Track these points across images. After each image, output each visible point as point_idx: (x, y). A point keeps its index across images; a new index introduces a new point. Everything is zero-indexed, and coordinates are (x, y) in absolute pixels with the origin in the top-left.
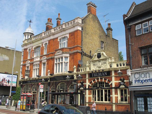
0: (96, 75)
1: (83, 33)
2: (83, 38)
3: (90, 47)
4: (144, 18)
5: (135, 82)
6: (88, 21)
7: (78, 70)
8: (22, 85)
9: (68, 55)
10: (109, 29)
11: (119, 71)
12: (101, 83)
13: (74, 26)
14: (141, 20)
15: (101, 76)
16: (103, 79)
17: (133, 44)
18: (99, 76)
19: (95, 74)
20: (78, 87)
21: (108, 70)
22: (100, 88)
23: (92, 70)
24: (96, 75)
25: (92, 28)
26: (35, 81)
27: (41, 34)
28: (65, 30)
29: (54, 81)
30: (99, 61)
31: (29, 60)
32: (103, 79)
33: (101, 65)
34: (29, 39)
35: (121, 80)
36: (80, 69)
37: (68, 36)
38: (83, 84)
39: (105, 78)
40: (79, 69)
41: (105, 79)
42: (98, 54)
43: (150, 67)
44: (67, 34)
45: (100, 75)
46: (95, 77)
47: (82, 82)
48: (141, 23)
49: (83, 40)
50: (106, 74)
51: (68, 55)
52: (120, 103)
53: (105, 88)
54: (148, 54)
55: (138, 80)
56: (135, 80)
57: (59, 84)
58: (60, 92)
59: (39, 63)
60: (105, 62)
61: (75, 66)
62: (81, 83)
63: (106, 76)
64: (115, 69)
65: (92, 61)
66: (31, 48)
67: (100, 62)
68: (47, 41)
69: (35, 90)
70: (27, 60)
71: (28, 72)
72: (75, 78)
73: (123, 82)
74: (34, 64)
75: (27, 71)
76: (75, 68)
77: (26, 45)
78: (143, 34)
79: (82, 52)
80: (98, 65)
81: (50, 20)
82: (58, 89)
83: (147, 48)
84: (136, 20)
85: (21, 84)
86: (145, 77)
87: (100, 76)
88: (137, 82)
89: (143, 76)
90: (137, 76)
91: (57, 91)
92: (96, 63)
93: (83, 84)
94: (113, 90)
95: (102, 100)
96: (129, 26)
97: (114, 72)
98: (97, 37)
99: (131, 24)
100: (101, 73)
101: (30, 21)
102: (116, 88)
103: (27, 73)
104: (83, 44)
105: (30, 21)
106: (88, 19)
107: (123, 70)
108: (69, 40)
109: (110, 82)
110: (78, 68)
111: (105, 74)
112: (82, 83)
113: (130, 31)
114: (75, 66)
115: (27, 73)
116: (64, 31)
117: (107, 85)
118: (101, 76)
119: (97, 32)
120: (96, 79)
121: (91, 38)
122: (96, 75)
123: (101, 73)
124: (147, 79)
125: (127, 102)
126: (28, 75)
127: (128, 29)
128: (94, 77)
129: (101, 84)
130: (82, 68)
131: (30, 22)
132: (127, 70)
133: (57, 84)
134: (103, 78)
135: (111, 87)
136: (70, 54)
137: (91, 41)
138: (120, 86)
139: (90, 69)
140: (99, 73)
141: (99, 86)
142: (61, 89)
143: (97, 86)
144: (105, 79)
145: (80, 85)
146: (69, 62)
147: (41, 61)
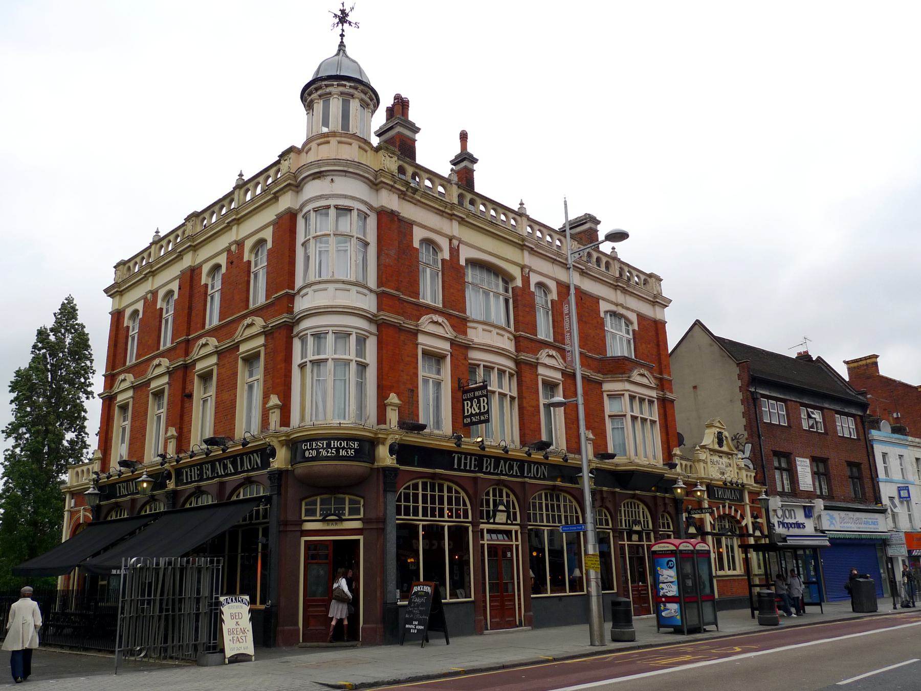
19: (487, 461)
30: (720, 453)
50: (546, 474)
67: (721, 457)
69: (508, 517)
80: (721, 466)
101: (343, 11)
126: (480, 414)
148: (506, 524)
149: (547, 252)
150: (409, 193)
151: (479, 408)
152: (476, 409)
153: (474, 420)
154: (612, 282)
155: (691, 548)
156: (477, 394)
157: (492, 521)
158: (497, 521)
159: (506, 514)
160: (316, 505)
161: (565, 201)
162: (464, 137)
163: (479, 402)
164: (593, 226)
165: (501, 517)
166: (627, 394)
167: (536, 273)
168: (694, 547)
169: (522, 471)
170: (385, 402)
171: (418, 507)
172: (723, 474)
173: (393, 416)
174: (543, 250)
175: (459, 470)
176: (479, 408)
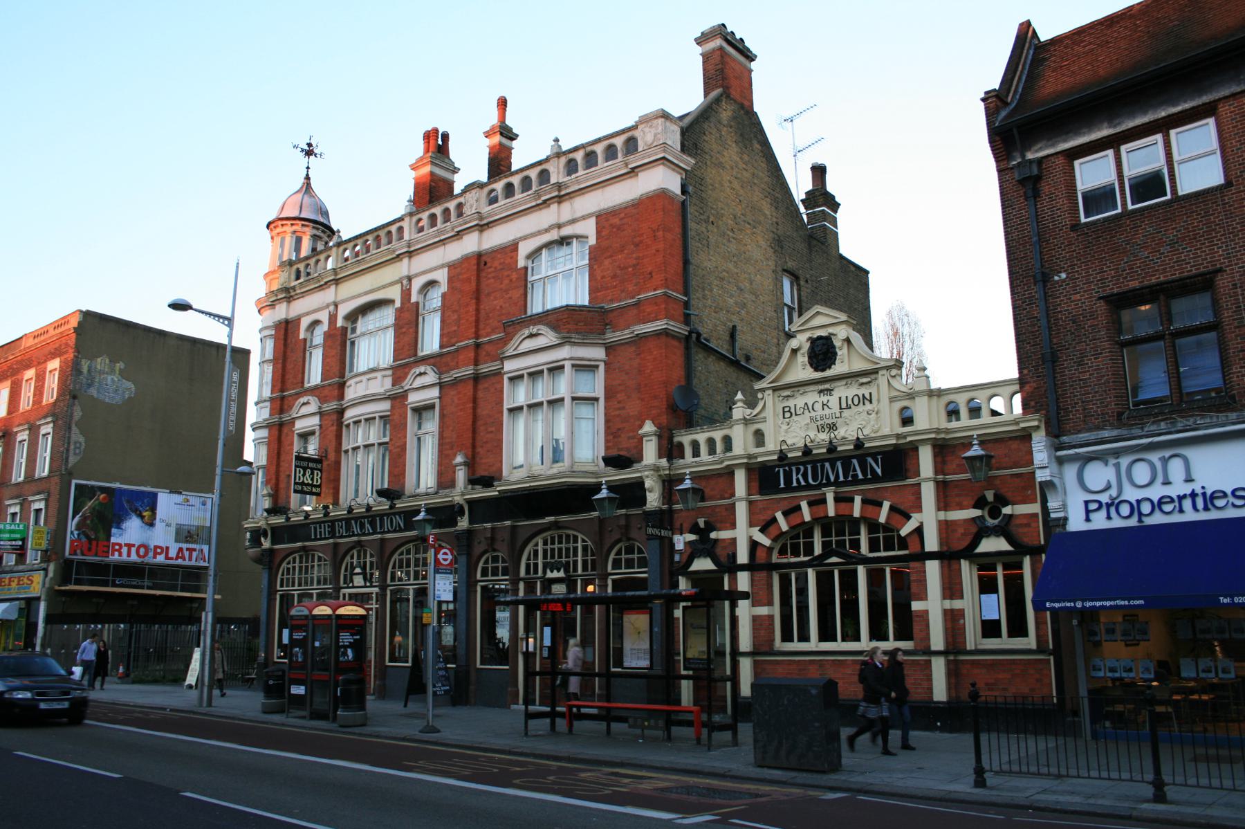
0: (805, 476)
1: (691, 210)
2: (693, 244)
3: (731, 301)
4: (1132, 115)
5: (1088, 512)
6: (711, 141)
7: (671, 450)
8: (271, 551)
9: (598, 353)
10: (821, 197)
11: (970, 445)
12: (845, 524)
13: (633, 169)
14: (1115, 127)
15: (842, 479)
16: (858, 500)
17: (1064, 276)
18: (829, 484)
19: (798, 471)
20: (677, 558)
21: (894, 442)
22: (834, 559)
23: (771, 445)
24: (805, 476)
25: (736, 185)
26: (362, 526)
27: (394, 229)
28: (571, 195)
29: (498, 524)
30: (825, 386)
31: (314, 390)
32: (858, 500)
33: (838, 411)
34: (307, 258)
35: (980, 503)
36: (685, 439)
37: (589, 228)
38: (713, 535)
39: (870, 496)
40: (676, 439)
41: (872, 503)
42: (813, 341)
43: (1192, 420)
44: (584, 218)
45: (837, 477)
46: (800, 488)
47: (702, 525)
48: (1113, 143)
49: (694, 259)
50: (879, 471)
51: (598, 353)
52: (980, 647)
53: (872, 555)
54: (1171, 334)
55: (1104, 498)
56: (1086, 503)
57: (534, 542)
58: (543, 592)
59: (385, 406)
60: (865, 391)
61: (649, 427)
62: (694, 529)
63: (876, 479)
64: (942, 436)
65: (775, 389)
66: (324, 316)
67: (830, 391)
68: (442, 266)
69: (365, 579)
70: (299, 395)
71: (312, 469)
72: (653, 500)
73: (995, 513)
74: (349, 414)
75: (305, 464)
76: (460, 464)
77: (288, 295)
78: (1126, 214)
79: (690, 332)
80: (819, 411)
81: (438, 145)
82: (528, 572)
83: (1162, 297)
84: (1084, 130)
85: (266, 544)
86: (1160, 479)
87: (837, 483)
88: (1103, 513)
89: (1141, 473)
90: (1098, 475)
91: (521, 585)
92: (799, 401)
93: (713, 535)
94: (933, 569)
95: (804, 638)
96: (1031, 161)
97: (935, 456)
98: (762, 243)
99: (1041, 149)
100: (839, 464)
101: (309, 145)
102: (948, 557)
103: (308, 472)
104: (694, 282)
105: (309, 145)
106: (714, 131)
107: (996, 441)
108: (596, 256)
109: (909, 518)
110: (671, 438)
111: (873, 470)
112: (703, 533)
113: (1036, 195)
114: (649, 427)
115: (308, 472)
116: (560, 199)
117: (885, 536)
118: (842, 479)
119: (765, 215)
120: (804, 505)
121: (733, 247)
122: (806, 479)
123: (839, 464)
124: (1173, 491)
125: (1031, 642)
126: (312, 485)
127: (1022, 182)
128: (789, 488)
129: (840, 533)
130: (702, 437)
131: (309, 153)
132: (270, 569)
133: (519, 543)
134: (858, 493)
135: (914, 548)
136: (609, 348)
137: (731, 266)
138: (976, 542)
139: (759, 437)
140: (827, 465)
141: (825, 545)
142: (550, 575)
143: (809, 549)
144: (872, 503)
145: (687, 544)
146: (607, 398)
147: (398, 399)
148: (365, 587)
149: (425, 241)
150: (293, 294)
151: (312, 479)
152: (309, 479)
153: (305, 489)
154: (534, 204)
155: (306, 612)
156: (311, 465)
157: (351, 585)
158: (356, 584)
159: (361, 576)
160: (899, 549)
161: (238, 263)
162: (503, 103)
163: (312, 473)
164: (505, 141)
165: (358, 580)
166: (568, 364)
167: (529, 238)
168: (334, 611)
169: (374, 528)
170: (640, 432)
171: (577, 561)
172: (832, 427)
173: (461, 476)
174: (421, 242)
175: (316, 539)
176: (312, 479)
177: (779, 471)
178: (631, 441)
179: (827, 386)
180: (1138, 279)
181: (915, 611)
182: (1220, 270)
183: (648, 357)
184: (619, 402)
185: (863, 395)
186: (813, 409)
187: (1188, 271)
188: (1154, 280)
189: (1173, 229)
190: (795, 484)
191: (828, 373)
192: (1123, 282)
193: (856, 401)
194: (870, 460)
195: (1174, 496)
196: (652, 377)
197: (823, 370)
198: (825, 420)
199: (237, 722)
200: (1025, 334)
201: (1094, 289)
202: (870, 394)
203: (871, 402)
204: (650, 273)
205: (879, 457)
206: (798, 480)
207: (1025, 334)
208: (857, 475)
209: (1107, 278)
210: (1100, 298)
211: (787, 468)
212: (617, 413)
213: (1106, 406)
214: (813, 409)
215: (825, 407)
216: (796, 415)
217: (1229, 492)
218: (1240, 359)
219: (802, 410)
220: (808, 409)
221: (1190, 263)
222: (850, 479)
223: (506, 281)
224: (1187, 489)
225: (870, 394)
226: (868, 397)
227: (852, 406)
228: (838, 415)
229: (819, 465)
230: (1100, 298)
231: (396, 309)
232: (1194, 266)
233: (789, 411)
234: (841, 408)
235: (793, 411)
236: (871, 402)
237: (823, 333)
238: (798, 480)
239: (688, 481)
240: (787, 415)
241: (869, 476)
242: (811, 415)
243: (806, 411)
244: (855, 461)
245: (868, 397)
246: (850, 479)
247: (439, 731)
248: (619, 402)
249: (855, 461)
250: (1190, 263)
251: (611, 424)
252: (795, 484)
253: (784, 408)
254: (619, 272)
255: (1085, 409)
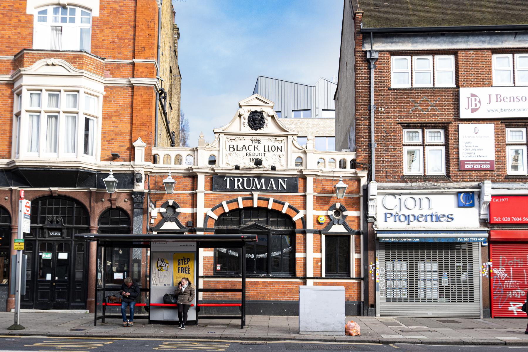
0: (243, 184)
15: (264, 188)
18: (257, 190)
19: (239, 180)
24: (243, 184)
39: (278, 199)
46: (239, 190)
50: (285, 187)
63: (283, 190)
87: (261, 190)
100: (263, 180)
118: (264, 188)
122: (243, 186)
123: (263, 180)
128: (232, 189)
177: (227, 179)
178: (122, 148)
179: (258, 138)
180: (416, 119)
181: (298, 258)
182: (450, 123)
183: (139, 99)
184: (113, 122)
185: (277, 147)
186: (248, 149)
187: (438, 120)
188: (423, 121)
189: (434, 100)
190: (236, 187)
191: (258, 131)
192: (410, 119)
193: (273, 149)
194: (280, 180)
195: (424, 215)
196: (142, 112)
197: (256, 129)
198: (255, 156)
199: (138, 339)
200: (361, 132)
201: (396, 119)
202: (281, 147)
203: (281, 151)
204: (144, 48)
205: (286, 180)
206: (238, 185)
207: (361, 132)
208: (273, 187)
209: (403, 115)
210: (399, 124)
211: (232, 178)
212: (112, 129)
213: (397, 172)
214: (248, 149)
215: (256, 149)
216: (237, 150)
217: (446, 215)
218: (454, 162)
219: (242, 148)
220: (246, 148)
221: (439, 117)
222: (268, 189)
223: (15, 20)
224: (429, 212)
225: (281, 147)
226: (280, 148)
227: (271, 151)
228: (263, 155)
229: (251, 179)
230: (399, 124)
231: (94, 20)
232: (441, 118)
233: (233, 148)
234: (265, 151)
235: (235, 147)
236: (281, 151)
237: (259, 109)
238: (238, 185)
239: (111, 176)
240: (232, 149)
241: (279, 189)
242: (247, 152)
243: (244, 150)
244: (272, 180)
245: (280, 148)
246: (268, 189)
247: (24, 328)
248: (113, 122)
249: (272, 180)
250: (439, 117)
251: (106, 135)
252: (236, 187)
253: (230, 145)
254: (116, 40)
255: (386, 172)
